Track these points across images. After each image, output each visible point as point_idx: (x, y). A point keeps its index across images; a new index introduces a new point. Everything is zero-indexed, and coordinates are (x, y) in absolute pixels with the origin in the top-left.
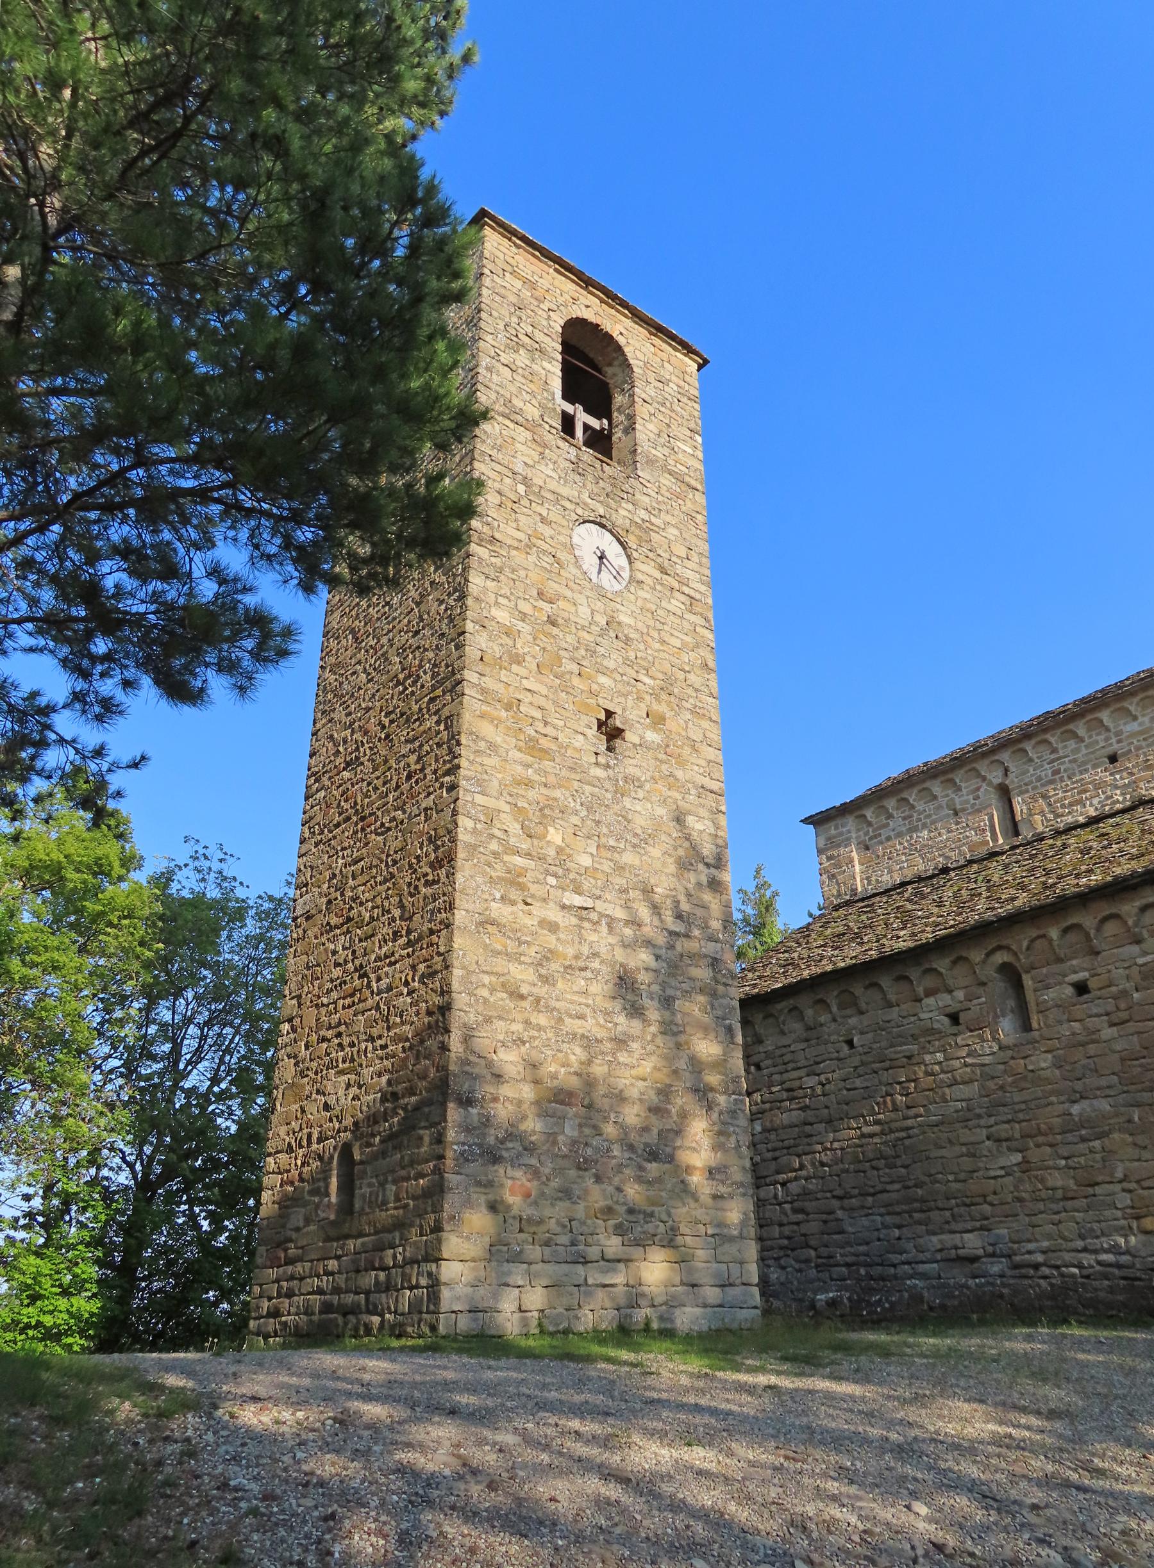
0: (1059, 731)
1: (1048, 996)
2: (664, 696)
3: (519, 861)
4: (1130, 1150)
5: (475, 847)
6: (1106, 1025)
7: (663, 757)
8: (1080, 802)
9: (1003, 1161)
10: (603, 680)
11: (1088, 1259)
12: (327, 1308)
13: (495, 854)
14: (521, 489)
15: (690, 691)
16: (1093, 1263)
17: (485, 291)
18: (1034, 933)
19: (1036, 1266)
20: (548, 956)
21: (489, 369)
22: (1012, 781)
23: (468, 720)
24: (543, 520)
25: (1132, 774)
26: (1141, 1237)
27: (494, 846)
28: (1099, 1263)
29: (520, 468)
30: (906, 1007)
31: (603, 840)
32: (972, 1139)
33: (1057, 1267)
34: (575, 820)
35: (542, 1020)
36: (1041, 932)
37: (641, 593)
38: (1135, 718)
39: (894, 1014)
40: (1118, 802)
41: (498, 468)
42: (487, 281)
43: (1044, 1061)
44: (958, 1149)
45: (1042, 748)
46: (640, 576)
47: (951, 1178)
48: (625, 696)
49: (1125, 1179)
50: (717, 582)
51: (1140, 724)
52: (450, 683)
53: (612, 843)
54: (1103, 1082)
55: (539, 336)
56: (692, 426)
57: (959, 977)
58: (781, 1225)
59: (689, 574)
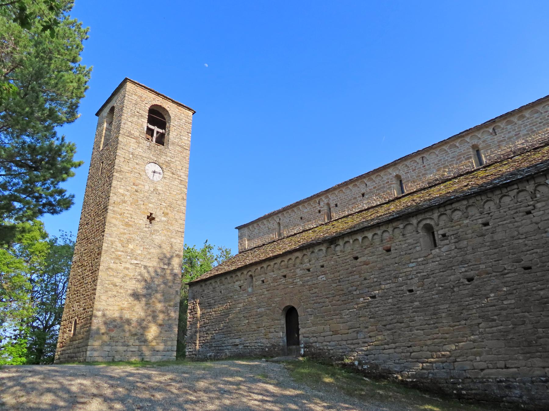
2: (169, 208)
3: (120, 253)
5: (107, 251)
8: (294, 229)
10: (150, 205)
11: (256, 344)
12: (69, 357)
13: (113, 252)
14: (131, 156)
15: (178, 206)
17: (125, 101)
19: (248, 346)
20: (126, 275)
21: (124, 124)
22: (281, 222)
23: (108, 219)
24: (137, 164)
27: (113, 250)
29: (131, 150)
31: (145, 247)
34: (138, 242)
35: (122, 291)
37: (165, 181)
39: (230, 285)
41: (124, 151)
42: (126, 98)
43: (254, 299)
46: (165, 176)
48: (157, 209)
50: (189, 176)
52: (106, 209)
53: (147, 247)
55: (141, 112)
56: (188, 131)
57: (242, 277)
59: (181, 174)
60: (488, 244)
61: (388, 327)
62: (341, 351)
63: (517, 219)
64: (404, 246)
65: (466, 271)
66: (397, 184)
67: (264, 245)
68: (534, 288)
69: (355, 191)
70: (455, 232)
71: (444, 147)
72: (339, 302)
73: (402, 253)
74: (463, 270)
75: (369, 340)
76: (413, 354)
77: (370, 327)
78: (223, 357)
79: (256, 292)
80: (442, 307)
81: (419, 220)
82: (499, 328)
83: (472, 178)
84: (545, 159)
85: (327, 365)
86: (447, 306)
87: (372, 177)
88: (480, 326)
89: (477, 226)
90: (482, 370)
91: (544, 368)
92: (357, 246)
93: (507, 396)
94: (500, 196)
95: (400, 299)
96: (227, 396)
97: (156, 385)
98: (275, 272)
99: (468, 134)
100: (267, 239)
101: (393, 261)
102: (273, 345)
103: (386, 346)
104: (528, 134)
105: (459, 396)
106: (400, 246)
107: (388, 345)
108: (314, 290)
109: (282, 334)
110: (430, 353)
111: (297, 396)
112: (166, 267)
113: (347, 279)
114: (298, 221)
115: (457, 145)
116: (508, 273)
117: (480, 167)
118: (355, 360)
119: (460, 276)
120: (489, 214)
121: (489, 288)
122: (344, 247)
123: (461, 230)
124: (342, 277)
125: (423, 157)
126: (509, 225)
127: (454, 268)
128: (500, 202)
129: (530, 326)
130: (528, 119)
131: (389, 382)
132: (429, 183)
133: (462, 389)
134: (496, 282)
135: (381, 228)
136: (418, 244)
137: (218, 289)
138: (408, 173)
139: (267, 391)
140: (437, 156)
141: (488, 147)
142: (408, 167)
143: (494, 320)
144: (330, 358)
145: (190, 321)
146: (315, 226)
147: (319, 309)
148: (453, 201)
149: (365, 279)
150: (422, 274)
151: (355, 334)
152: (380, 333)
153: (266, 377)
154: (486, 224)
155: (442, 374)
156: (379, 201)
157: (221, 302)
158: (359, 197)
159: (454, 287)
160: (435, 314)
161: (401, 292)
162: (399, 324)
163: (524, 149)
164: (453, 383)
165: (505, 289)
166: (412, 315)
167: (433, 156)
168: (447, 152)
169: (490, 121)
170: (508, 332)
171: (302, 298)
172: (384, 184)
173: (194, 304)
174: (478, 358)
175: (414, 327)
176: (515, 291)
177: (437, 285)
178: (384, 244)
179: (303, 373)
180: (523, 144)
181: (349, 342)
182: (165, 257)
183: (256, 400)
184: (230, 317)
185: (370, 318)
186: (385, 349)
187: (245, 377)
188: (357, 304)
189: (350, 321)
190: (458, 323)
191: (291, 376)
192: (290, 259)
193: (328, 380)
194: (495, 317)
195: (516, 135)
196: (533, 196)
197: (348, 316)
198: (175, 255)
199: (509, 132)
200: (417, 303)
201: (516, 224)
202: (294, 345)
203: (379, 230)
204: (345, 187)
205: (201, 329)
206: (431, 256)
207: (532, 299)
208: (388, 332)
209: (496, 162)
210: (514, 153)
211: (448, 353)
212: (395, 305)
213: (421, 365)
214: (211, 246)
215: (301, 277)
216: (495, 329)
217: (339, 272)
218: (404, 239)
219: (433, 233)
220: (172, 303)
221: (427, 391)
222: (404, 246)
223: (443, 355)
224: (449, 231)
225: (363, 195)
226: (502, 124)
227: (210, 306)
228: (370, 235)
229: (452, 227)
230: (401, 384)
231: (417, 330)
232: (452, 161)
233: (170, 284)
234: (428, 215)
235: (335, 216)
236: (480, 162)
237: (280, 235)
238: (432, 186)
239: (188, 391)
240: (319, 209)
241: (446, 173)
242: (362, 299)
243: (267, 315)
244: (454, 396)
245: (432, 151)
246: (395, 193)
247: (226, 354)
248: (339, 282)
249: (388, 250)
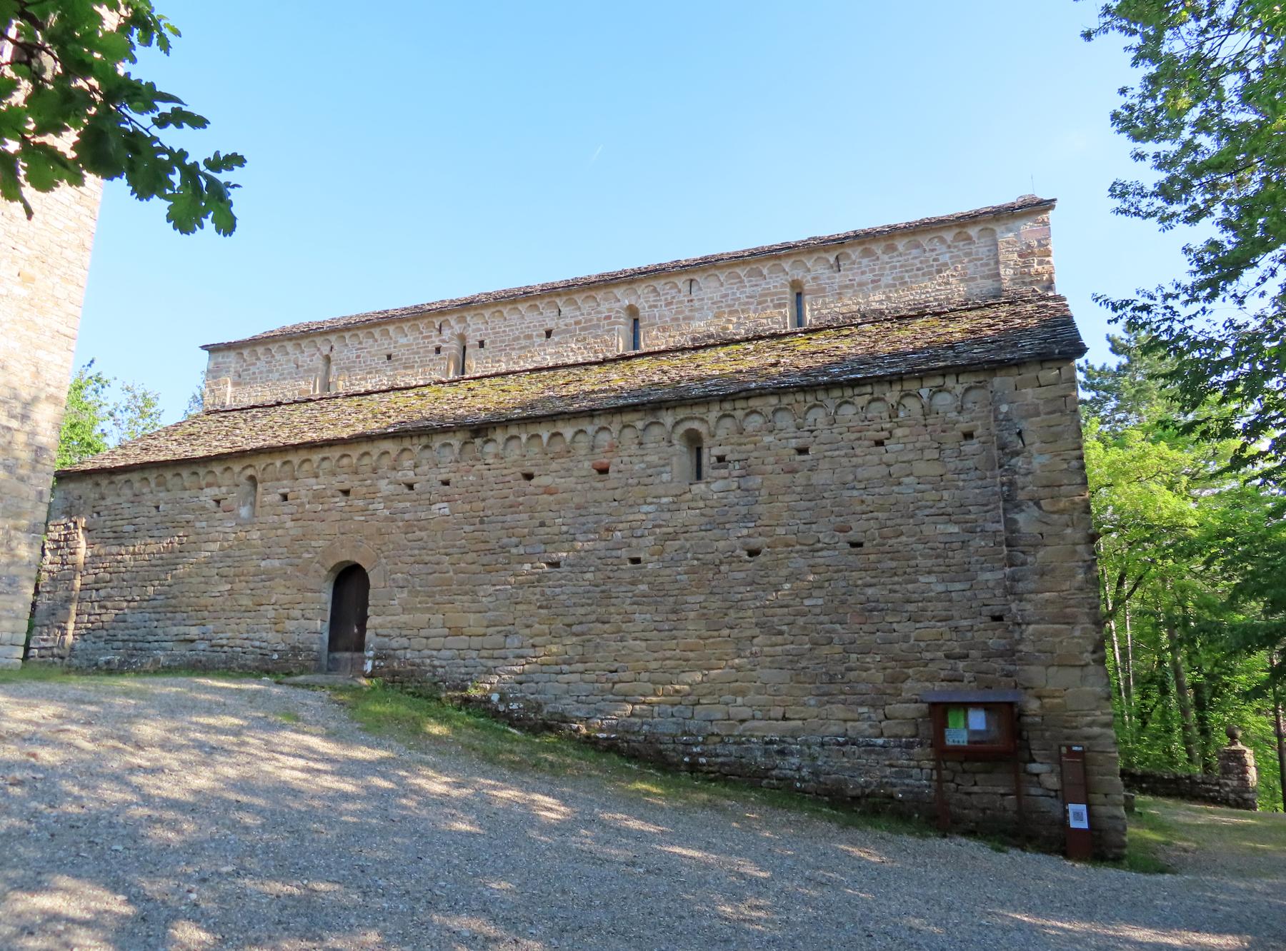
1: (267, 499)
2: (37, 263)
7: (26, 306)
8: (365, 379)
9: (221, 588)
15: (63, 262)
18: (269, 461)
19: (222, 646)
22: (333, 355)
30: (194, 492)
39: (186, 494)
43: (255, 535)
45: (354, 339)
54: (280, 550)
57: (226, 479)
58: (90, 615)
60: (799, 489)
61: (575, 628)
62: (463, 670)
63: (858, 451)
64: (637, 467)
65: (749, 536)
66: (626, 324)
67: (279, 404)
68: (860, 582)
69: (531, 319)
70: (744, 456)
71: (738, 270)
73: (630, 481)
74: (745, 532)
75: (531, 652)
76: (617, 686)
77: (537, 626)
78: (148, 667)
79: (261, 519)
81: (678, 418)
82: (787, 647)
83: (783, 350)
84: (918, 344)
85: (426, 698)
86: (702, 598)
87: (575, 297)
88: (755, 641)
89: (785, 451)
90: (742, 721)
91: (845, 721)
92: (536, 450)
93: (776, 767)
94: (838, 401)
95: (611, 575)
96: (222, 759)
97: (26, 731)
98: (322, 479)
100: (289, 391)
101: (609, 494)
102: (293, 648)
103: (565, 668)
104: (895, 286)
105: (693, 768)
107: (570, 664)
108: (418, 533)
109: (320, 625)
110: (651, 686)
111: (381, 762)
112: (14, 424)
113: (500, 518)
114: (380, 361)
115: (765, 271)
116: (821, 549)
117: (798, 329)
118: (491, 690)
119: (738, 543)
120: (812, 431)
121: (784, 572)
122: (504, 449)
123: (755, 454)
124: (490, 513)
125: (691, 280)
126: (843, 460)
127: (727, 526)
128: (836, 412)
129: (839, 648)
130: (901, 255)
131: (560, 738)
132: (694, 339)
133: (701, 755)
134: (799, 562)
135: (596, 421)
136: (668, 468)
137: (149, 500)
138: (655, 306)
139: (309, 749)
140: (722, 285)
141: (820, 291)
143: (781, 633)
144: (435, 684)
145: (50, 572)
146: (421, 383)
147: (424, 576)
148: (752, 393)
149: (542, 524)
150: (665, 530)
151: (500, 638)
152: (557, 640)
153: (294, 719)
154: (802, 451)
155: (667, 727)
156: (581, 357)
157: (156, 533)
159: (721, 563)
160: (675, 612)
161: (616, 561)
162: (600, 625)
163: (882, 313)
164: (686, 744)
165: (811, 578)
166: (629, 609)
167: (713, 283)
168: (742, 282)
170: (801, 655)
171: (384, 548)
172: (599, 319)
173: (68, 528)
174: (739, 700)
175: (630, 633)
176: (826, 584)
177: (689, 555)
179: (379, 713)
180: (881, 302)
181: (484, 653)
182: (16, 397)
183: (293, 768)
184: (180, 571)
185: (540, 607)
186: (561, 673)
187: (246, 718)
188: (515, 575)
189: (494, 610)
190: (716, 633)
191: (353, 719)
192: (366, 454)
193: (436, 729)
194: (785, 628)
195: (873, 282)
196: (893, 415)
197: (489, 599)
198: (43, 396)
199: (863, 273)
200: (643, 587)
201: (854, 459)
202: (347, 650)
203: (592, 423)
204: (510, 307)
205: (83, 595)
206: (688, 496)
207: (851, 600)
208: (574, 639)
209: (829, 327)
210: (864, 316)
211: (686, 687)
212: (597, 586)
213: (630, 707)
214: (105, 377)
215: (386, 499)
216: (779, 649)
217: (484, 500)
219: (699, 450)
220: (24, 522)
221: (635, 757)
222: (637, 467)
223: (677, 691)
224: (732, 452)
225: (549, 334)
226: (854, 253)
227: (119, 537)
228: (568, 431)
229: (740, 444)
230: (585, 743)
231: (635, 639)
232: (747, 303)
233: (22, 472)
234: (698, 411)
235: (474, 368)
236: (799, 320)
237: (326, 386)
238: (701, 347)
239: (121, 745)
240: (438, 343)
241: (731, 326)
242: (527, 567)
243: (285, 576)
244: (683, 767)
245: (713, 271)
246: (621, 345)
247: (157, 661)
248: (482, 522)
249: (603, 471)
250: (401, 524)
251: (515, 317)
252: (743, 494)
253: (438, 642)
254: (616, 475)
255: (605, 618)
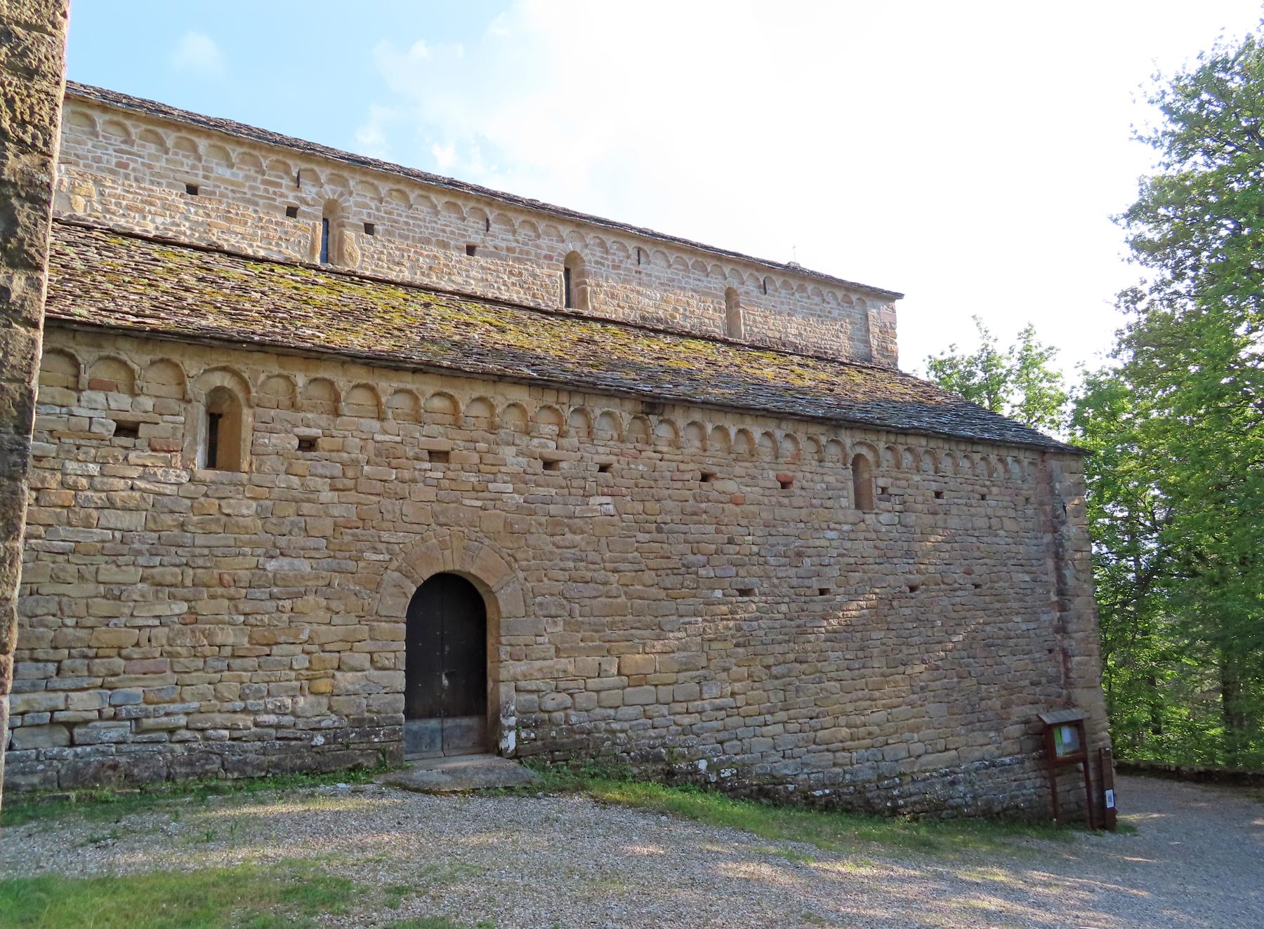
0: (143, 127)
4: (321, 613)
6: (327, 488)
9: (160, 610)
11: (245, 720)
16: (250, 724)
18: (276, 370)
19: (172, 731)
25: (208, 216)
26: (311, 698)
28: (256, 724)
32: (119, 578)
33: (202, 730)
36: (285, 373)
38: (231, 166)
40: (185, 234)
44: (90, 588)
47: (71, 622)
49: (310, 641)
51: (233, 174)
54: (311, 543)
57: (156, 382)
72: (653, 590)
73: (814, 501)
77: (735, 668)
80: (875, 635)
98: (391, 424)
99: (271, 150)
102: (359, 722)
106: (811, 484)
108: (569, 536)
124: (668, 519)
132: (643, 318)
133: (899, 797)
135: (784, 425)
140: (670, 266)
142: (607, 252)
154: (938, 495)
155: (865, 773)
158: (459, 248)
164: (888, 788)
169: (706, 247)
171: (519, 555)
178: (780, 467)
185: (737, 645)
186: (766, 725)
202: (431, 715)
212: (791, 620)
215: (515, 477)
218: (820, 470)
248: (659, 530)
250: (543, 519)
251: (423, 210)
252: (904, 529)
253: (614, 697)
254: (798, 492)
255: (802, 656)
